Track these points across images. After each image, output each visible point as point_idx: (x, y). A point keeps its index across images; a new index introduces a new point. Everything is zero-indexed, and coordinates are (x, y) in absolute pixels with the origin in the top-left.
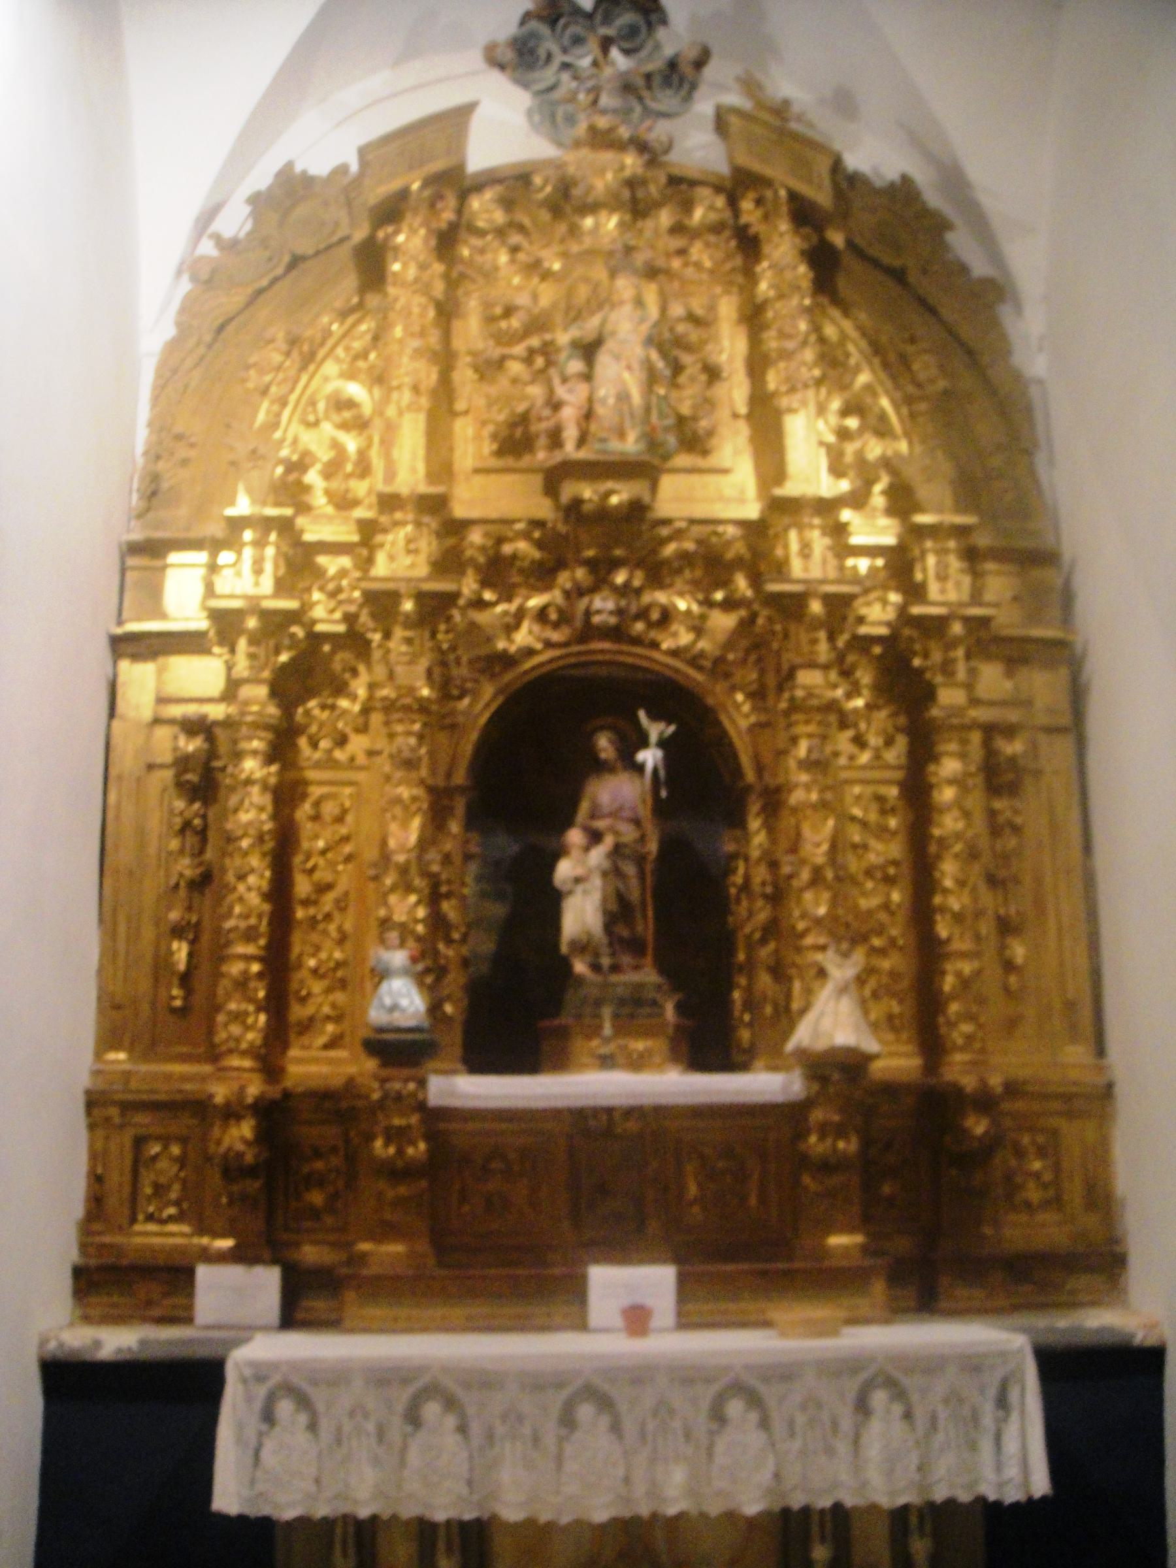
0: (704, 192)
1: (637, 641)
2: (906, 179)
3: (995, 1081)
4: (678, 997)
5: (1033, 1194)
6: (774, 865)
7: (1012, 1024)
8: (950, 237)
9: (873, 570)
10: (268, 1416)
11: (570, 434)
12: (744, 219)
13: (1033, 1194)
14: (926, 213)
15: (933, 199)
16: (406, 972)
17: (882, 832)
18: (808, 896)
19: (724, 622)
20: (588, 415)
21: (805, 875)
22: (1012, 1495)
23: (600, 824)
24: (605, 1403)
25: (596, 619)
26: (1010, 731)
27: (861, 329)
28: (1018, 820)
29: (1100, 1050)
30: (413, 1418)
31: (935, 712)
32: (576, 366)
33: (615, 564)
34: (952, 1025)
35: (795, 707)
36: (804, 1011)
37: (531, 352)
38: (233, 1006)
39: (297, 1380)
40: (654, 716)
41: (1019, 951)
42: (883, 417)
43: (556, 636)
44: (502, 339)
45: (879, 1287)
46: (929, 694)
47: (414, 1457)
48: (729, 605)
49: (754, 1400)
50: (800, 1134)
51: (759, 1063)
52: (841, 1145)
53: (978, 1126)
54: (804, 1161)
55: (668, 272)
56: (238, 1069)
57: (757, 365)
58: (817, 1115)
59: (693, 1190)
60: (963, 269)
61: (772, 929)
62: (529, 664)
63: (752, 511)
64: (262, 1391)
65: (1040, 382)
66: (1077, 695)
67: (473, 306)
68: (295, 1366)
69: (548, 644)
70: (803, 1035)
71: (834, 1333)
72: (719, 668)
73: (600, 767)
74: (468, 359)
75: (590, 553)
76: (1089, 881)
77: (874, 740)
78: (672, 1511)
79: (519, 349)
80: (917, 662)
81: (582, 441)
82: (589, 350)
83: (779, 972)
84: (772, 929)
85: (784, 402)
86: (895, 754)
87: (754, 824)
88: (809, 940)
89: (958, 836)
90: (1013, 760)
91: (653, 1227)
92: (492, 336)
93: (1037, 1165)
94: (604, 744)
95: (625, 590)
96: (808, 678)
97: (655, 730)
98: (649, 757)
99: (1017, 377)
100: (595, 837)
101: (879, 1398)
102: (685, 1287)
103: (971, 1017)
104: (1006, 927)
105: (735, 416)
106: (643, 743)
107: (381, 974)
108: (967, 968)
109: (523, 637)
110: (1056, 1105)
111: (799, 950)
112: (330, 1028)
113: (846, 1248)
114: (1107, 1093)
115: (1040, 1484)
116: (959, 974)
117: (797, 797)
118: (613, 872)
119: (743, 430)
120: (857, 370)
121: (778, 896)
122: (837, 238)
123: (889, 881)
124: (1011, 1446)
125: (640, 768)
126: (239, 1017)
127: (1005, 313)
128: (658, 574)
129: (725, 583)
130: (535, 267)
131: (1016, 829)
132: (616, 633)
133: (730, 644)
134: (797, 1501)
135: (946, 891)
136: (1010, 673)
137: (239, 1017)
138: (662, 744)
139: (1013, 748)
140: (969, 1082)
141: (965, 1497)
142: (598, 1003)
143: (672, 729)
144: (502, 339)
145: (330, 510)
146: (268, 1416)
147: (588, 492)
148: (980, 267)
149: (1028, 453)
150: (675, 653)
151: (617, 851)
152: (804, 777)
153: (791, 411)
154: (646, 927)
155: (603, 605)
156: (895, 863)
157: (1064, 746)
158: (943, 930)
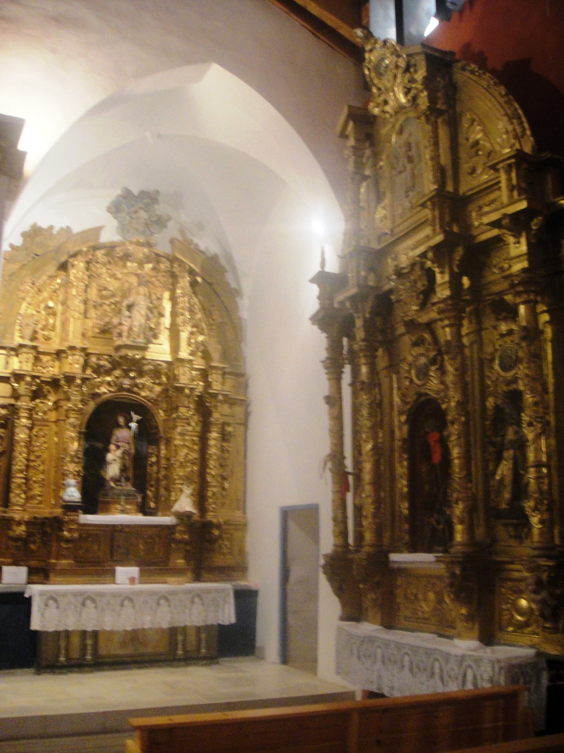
0: (164, 260)
2: (216, 255)
3: (221, 521)
5: (225, 551)
6: (168, 459)
7: (223, 504)
9: (197, 374)
10: (46, 605)
11: (125, 334)
12: (175, 270)
13: (225, 551)
14: (222, 267)
15: (223, 262)
16: (75, 486)
17: (192, 450)
19: (158, 389)
20: (130, 329)
22: (227, 623)
23: (119, 444)
24: (131, 600)
25: (125, 386)
26: (229, 424)
27: (200, 301)
28: (229, 449)
29: (244, 512)
30: (83, 604)
31: (212, 419)
32: (127, 313)
33: (131, 370)
34: (210, 505)
35: (179, 417)
36: (176, 501)
38: (17, 492)
39: (93, 596)
40: (136, 413)
41: (226, 485)
42: (203, 329)
43: (111, 389)
44: (102, 297)
45: (189, 574)
47: (84, 615)
48: (159, 384)
49: (167, 599)
50: (174, 533)
51: (160, 513)
53: (216, 532)
54: (174, 540)
55: (152, 283)
56: (17, 510)
57: (174, 314)
58: (179, 528)
59: (141, 547)
60: (228, 284)
61: (166, 477)
63: (169, 358)
64: (45, 598)
66: (247, 415)
67: (94, 285)
68: (54, 591)
69: (110, 391)
71: (182, 584)
72: (155, 402)
73: (119, 426)
74: (93, 303)
75: (125, 368)
76: (245, 465)
77: (193, 424)
80: (208, 404)
81: (128, 337)
82: (130, 307)
83: (168, 489)
84: (166, 477)
85: (181, 328)
86: (198, 429)
87: (163, 447)
88: (177, 482)
89: (215, 454)
90: (230, 432)
91: (131, 556)
92: (100, 296)
93: (227, 543)
94: (121, 420)
95: (133, 378)
96: (182, 410)
97: (135, 417)
98: (133, 425)
99: (240, 319)
100: (118, 447)
102: (142, 573)
103: (215, 503)
104: (224, 478)
106: (131, 420)
107: (69, 486)
108: (214, 489)
109: (103, 389)
110: (233, 527)
111: (174, 484)
112: (39, 498)
113: (181, 563)
114: (245, 525)
116: (212, 491)
117: (177, 442)
118: (123, 458)
120: (197, 314)
121: (168, 468)
122: (199, 279)
123: (194, 464)
124: (227, 611)
125: (130, 428)
126: (18, 495)
127: (238, 300)
128: (141, 374)
129: (159, 378)
130: (113, 276)
131: (228, 451)
132: (129, 390)
133: (158, 396)
134: (177, 624)
136: (230, 408)
137: (18, 495)
138: (138, 422)
139: (229, 429)
140: (215, 521)
141: (215, 623)
142: (119, 495)
143: (141, 418)
144: (102, 297)
145: (43, 340)
146: (46, 605)
147: (130, 353)
148: (233, 285)
149: (240, 342)
150: (144, 397)
151: (124, 453)
152: (178, 437)
153: (183, 331)
154: (130, 474)
155: (126, 383)
156: (195, 459)
157: (242, 428)
158: (209, 479)
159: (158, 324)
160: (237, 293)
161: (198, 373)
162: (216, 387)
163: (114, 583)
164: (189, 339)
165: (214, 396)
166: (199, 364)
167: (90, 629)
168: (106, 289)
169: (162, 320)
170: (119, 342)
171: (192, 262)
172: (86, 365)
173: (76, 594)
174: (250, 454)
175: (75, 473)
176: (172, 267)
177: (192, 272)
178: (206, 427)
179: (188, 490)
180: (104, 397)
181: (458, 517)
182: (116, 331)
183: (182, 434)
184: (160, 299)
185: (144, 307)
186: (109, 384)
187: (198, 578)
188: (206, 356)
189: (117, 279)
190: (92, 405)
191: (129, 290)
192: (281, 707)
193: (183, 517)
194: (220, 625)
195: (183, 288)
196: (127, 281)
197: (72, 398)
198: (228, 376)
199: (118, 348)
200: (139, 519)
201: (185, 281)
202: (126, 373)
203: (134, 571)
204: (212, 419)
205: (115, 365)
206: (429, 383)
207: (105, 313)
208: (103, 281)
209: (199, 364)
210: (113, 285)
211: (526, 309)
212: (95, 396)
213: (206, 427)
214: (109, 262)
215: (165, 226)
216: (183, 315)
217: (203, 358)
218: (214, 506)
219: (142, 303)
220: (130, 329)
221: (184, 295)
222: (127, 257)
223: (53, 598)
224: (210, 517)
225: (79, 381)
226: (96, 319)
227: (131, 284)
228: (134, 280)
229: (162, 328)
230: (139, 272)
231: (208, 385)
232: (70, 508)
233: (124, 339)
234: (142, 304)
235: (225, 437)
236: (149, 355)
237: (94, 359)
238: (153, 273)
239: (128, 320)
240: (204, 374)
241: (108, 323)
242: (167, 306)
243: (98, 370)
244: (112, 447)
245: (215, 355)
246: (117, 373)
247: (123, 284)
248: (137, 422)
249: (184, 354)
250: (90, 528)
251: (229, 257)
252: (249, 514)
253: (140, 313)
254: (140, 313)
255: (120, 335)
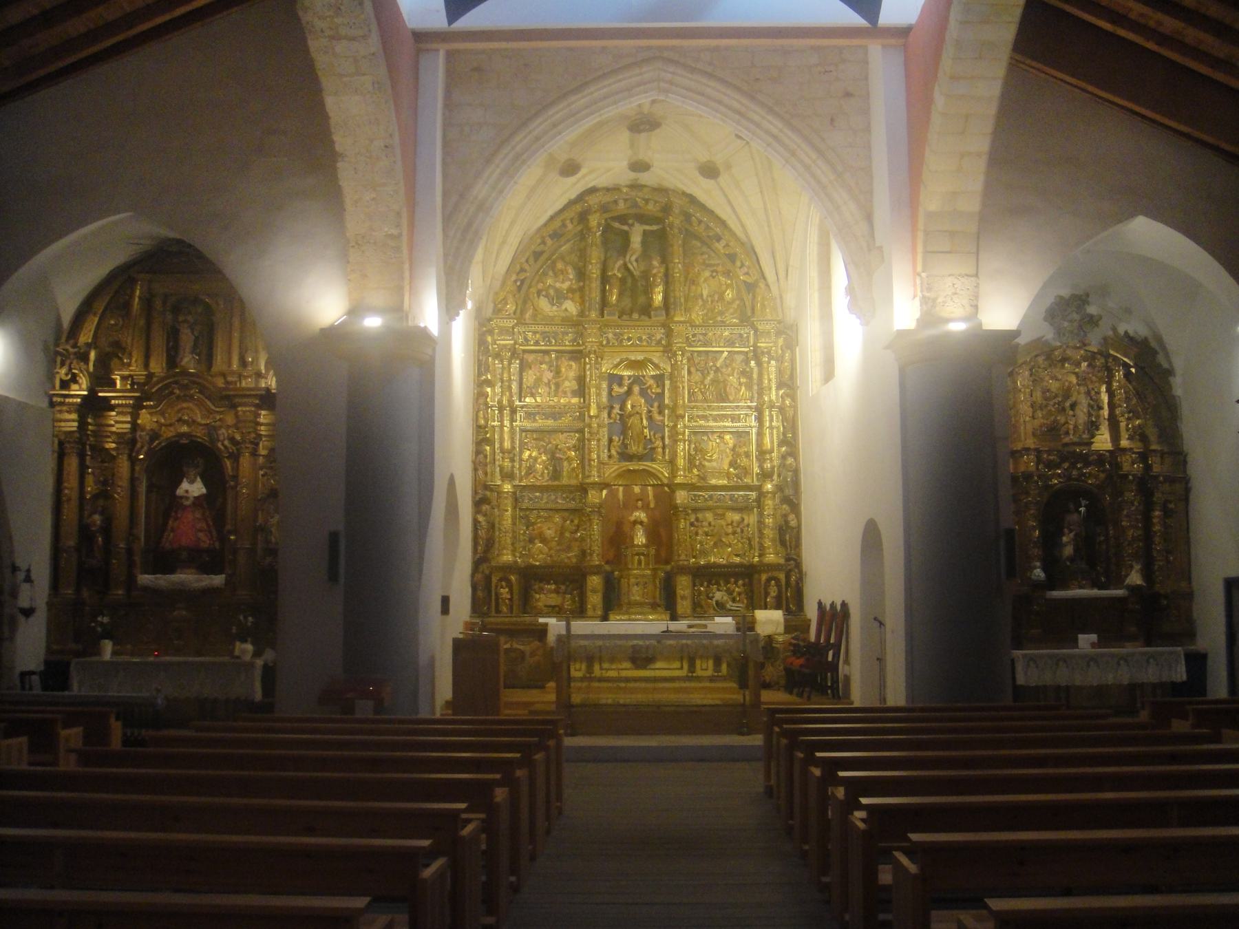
1: (1083, 481)
4: (140, 412)
8: (1158, 356)
11: (1071, 432)
12: (1109, 364)
15: (1153, 344)
18: (1127, 548)
19: (1102, 476)
21: (1127, 543)
26: (1170, 502)
29: (1189, 579)
37: (1055, 404)
46: (1152, 494)
49: (1126, 661)
52: (1137, 606)
57: (1112, 406)
62: (1055, 488)
63: (1109, 446)
65: (1179, 397)
66: (1187, 490)
69: (1060, 482)
70: (1128, 581)
78: (1110, 683)
79: (1051, 403)
82: (1073, 406)
86: (1141, 508)
94: (1072, 506)
96: (1127, 494)
97: (1084, 502)
98: (1082, 509)
99: (1174, 397)
100: (1071, 531)
101: (1151, 660)
105: (1105, 419)
107: (1035, 568)
115: (1185, 678)
119: (1107, 423)
127: (1171, 379)
128: (1087, 464)
130: (1055, 378)
135: (1156, 544)
139: (1171, 506)
140: (1162, 592)
143: (1087, 502)
144: (1046, 399)
148: (1166, 365)
152: (1125, 519)
156: (1140, 535)
158: (1155, 554)
159: (1098, 417)
160: (1170, 372)
161: (1137, 455)
162: (1156, 469)
163: (1077, 647)
164: (1127, 425)
165: (1156, 477)
166: (1137, 446)
167: (1064, 684)
168: (1048, 390)
169: (1101, 412)
170: (1066, 440)
171: (1126, 357)
174: (1192, 528)
176: (1107, 362)
177: (1126, 366)
178: (1148, 506)
179: (1137, 567)
182: (1064, 429)
183: (1127, 516)
184: (1098, 393)
185: (1086, 405)
187: (1148, 644)
188: (1144, 438)
189: (1057, 380)
191: (1069, 389)
193: (1134, 589)
194: (1172, 682)
195: (1119, 381)
196: (1067, 381)
197: (1032, 492)
198: (1166, 455)
199: (1066, 445)
200: (1095, 592)
201: (1119, 375)
202: (1073, 465)
203: (1093, 637)
204: (1155, 499)
205: (1063, 459)
208: (1045, 384)
209: (1137, 446)
210: (1054, 385)
213: (1148, 506)
214: (1050, 366)
215: (1097, 325)
216: (1120, 406)
217: (1141, 441)
218: (1161, 578)
219: (1084, 401)
220: (1076, 427)
221: (1120, 388)
222: (1064, 360)
223: (1031, 659)
224: (1157, 587)
226: (1043, 418)
227: (1070, 382)
228: (1074, 380)
229: (1102, 419)
230: (1077, 370)
231: (1148, 468)
232: (1038, 586)
233: (1071, 437)
234: (1084, 401)
235: (1167, 513)
236: (1096, 447)
238: (1090, 370)
239: (1074, 418)
240: (1143, 457)
242: (1105, 398)
243: (1050, 465)
244: (1066, 530)
245: (1153, 438)
246: (1066, 465)
247: (1064, 383)
248: (1085, 507)
249: (1124, 443)
250: (638, 685)
251: (1160, 340)
252: (1194, 584)
253: (1082, 411)
254: (1082, 411)
255: (1067, 433)
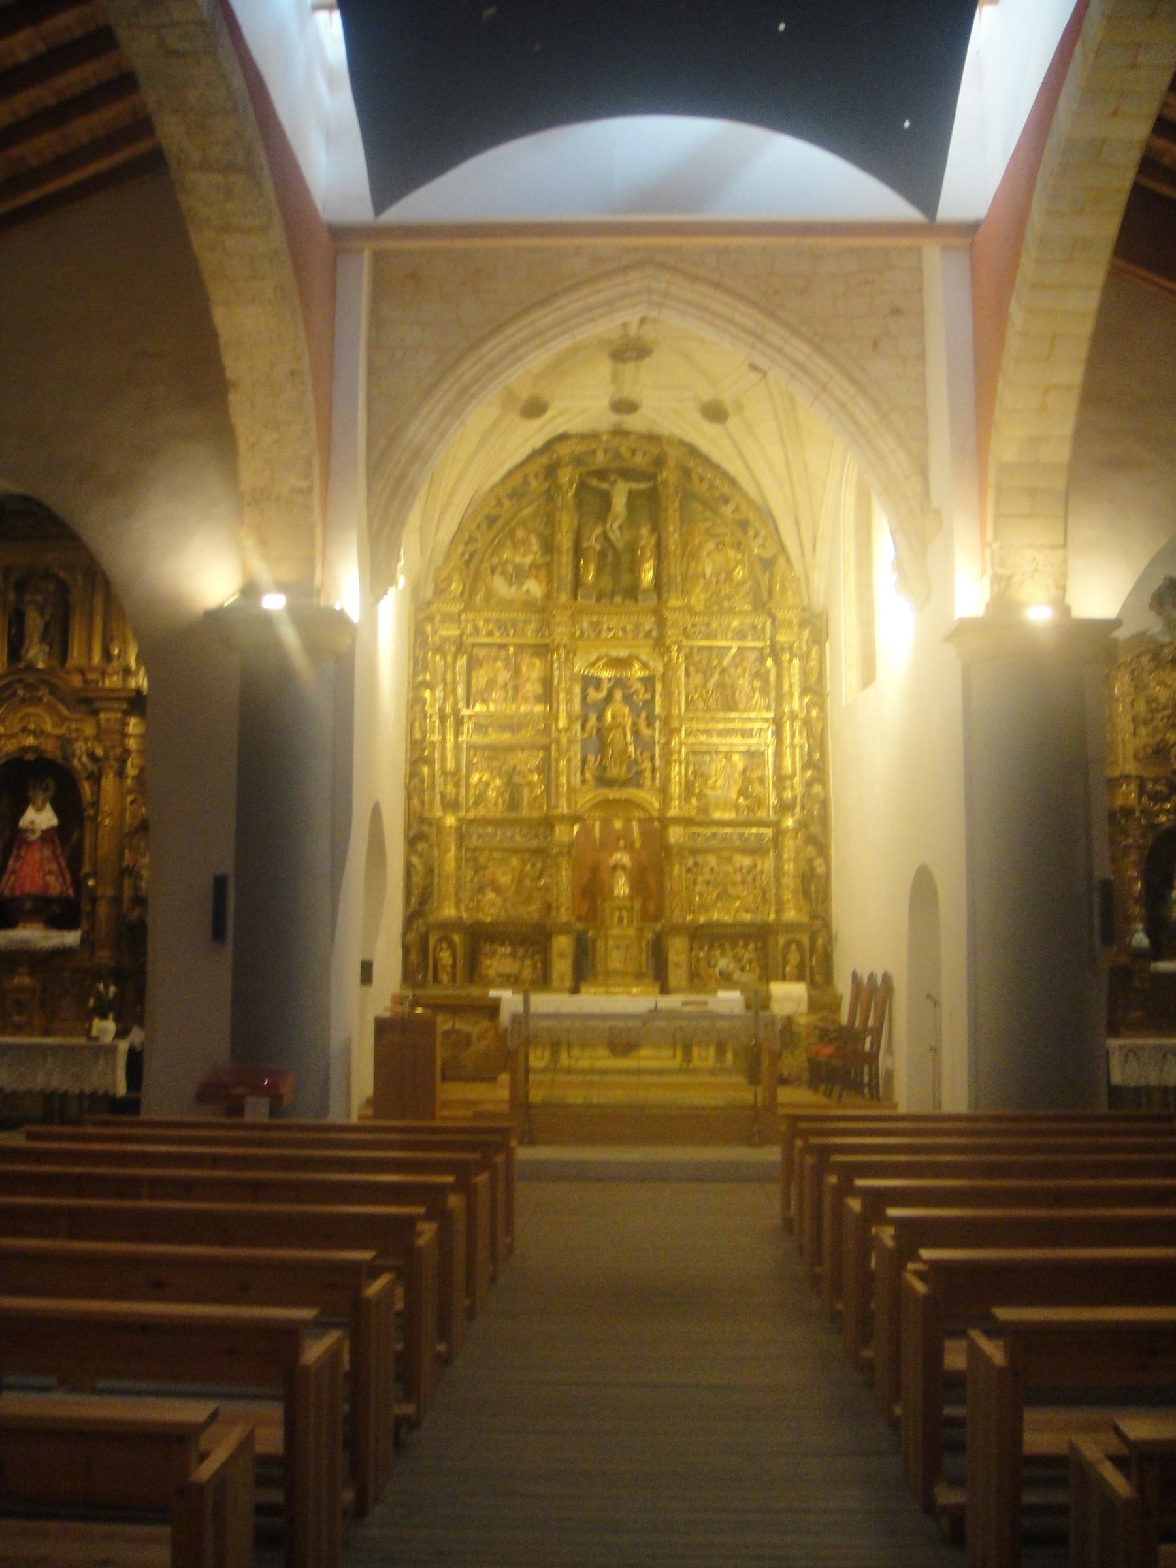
107: (1136, 931)
109: (1163, 818)
130: (1163, 683)
144: (1152, 711)
168: (1155, 700)
172: (1142, 791)
173: (1159, 1048)
175: (99, 704)
180: (1164, 827)
181: (793, 815)
186: (1168, 811)
190: (1150, 838)
192: (353, 740)
206: (675, 765)
207: (1156, 729)
211: (428, 770)
212: (1153, 826)
223: (1133, 1052)
225: (1138, 814)
237: (1150, 786)
241: (1163, 740)
243: (1156, 797)
